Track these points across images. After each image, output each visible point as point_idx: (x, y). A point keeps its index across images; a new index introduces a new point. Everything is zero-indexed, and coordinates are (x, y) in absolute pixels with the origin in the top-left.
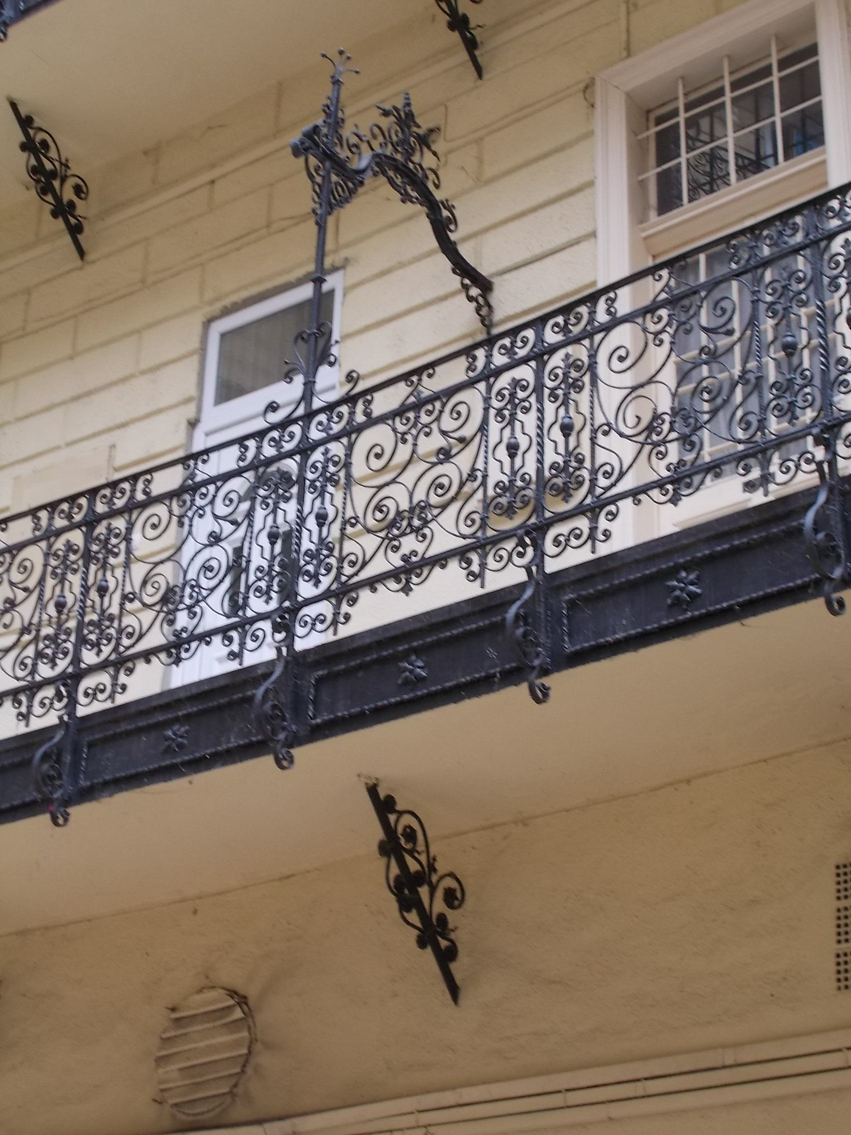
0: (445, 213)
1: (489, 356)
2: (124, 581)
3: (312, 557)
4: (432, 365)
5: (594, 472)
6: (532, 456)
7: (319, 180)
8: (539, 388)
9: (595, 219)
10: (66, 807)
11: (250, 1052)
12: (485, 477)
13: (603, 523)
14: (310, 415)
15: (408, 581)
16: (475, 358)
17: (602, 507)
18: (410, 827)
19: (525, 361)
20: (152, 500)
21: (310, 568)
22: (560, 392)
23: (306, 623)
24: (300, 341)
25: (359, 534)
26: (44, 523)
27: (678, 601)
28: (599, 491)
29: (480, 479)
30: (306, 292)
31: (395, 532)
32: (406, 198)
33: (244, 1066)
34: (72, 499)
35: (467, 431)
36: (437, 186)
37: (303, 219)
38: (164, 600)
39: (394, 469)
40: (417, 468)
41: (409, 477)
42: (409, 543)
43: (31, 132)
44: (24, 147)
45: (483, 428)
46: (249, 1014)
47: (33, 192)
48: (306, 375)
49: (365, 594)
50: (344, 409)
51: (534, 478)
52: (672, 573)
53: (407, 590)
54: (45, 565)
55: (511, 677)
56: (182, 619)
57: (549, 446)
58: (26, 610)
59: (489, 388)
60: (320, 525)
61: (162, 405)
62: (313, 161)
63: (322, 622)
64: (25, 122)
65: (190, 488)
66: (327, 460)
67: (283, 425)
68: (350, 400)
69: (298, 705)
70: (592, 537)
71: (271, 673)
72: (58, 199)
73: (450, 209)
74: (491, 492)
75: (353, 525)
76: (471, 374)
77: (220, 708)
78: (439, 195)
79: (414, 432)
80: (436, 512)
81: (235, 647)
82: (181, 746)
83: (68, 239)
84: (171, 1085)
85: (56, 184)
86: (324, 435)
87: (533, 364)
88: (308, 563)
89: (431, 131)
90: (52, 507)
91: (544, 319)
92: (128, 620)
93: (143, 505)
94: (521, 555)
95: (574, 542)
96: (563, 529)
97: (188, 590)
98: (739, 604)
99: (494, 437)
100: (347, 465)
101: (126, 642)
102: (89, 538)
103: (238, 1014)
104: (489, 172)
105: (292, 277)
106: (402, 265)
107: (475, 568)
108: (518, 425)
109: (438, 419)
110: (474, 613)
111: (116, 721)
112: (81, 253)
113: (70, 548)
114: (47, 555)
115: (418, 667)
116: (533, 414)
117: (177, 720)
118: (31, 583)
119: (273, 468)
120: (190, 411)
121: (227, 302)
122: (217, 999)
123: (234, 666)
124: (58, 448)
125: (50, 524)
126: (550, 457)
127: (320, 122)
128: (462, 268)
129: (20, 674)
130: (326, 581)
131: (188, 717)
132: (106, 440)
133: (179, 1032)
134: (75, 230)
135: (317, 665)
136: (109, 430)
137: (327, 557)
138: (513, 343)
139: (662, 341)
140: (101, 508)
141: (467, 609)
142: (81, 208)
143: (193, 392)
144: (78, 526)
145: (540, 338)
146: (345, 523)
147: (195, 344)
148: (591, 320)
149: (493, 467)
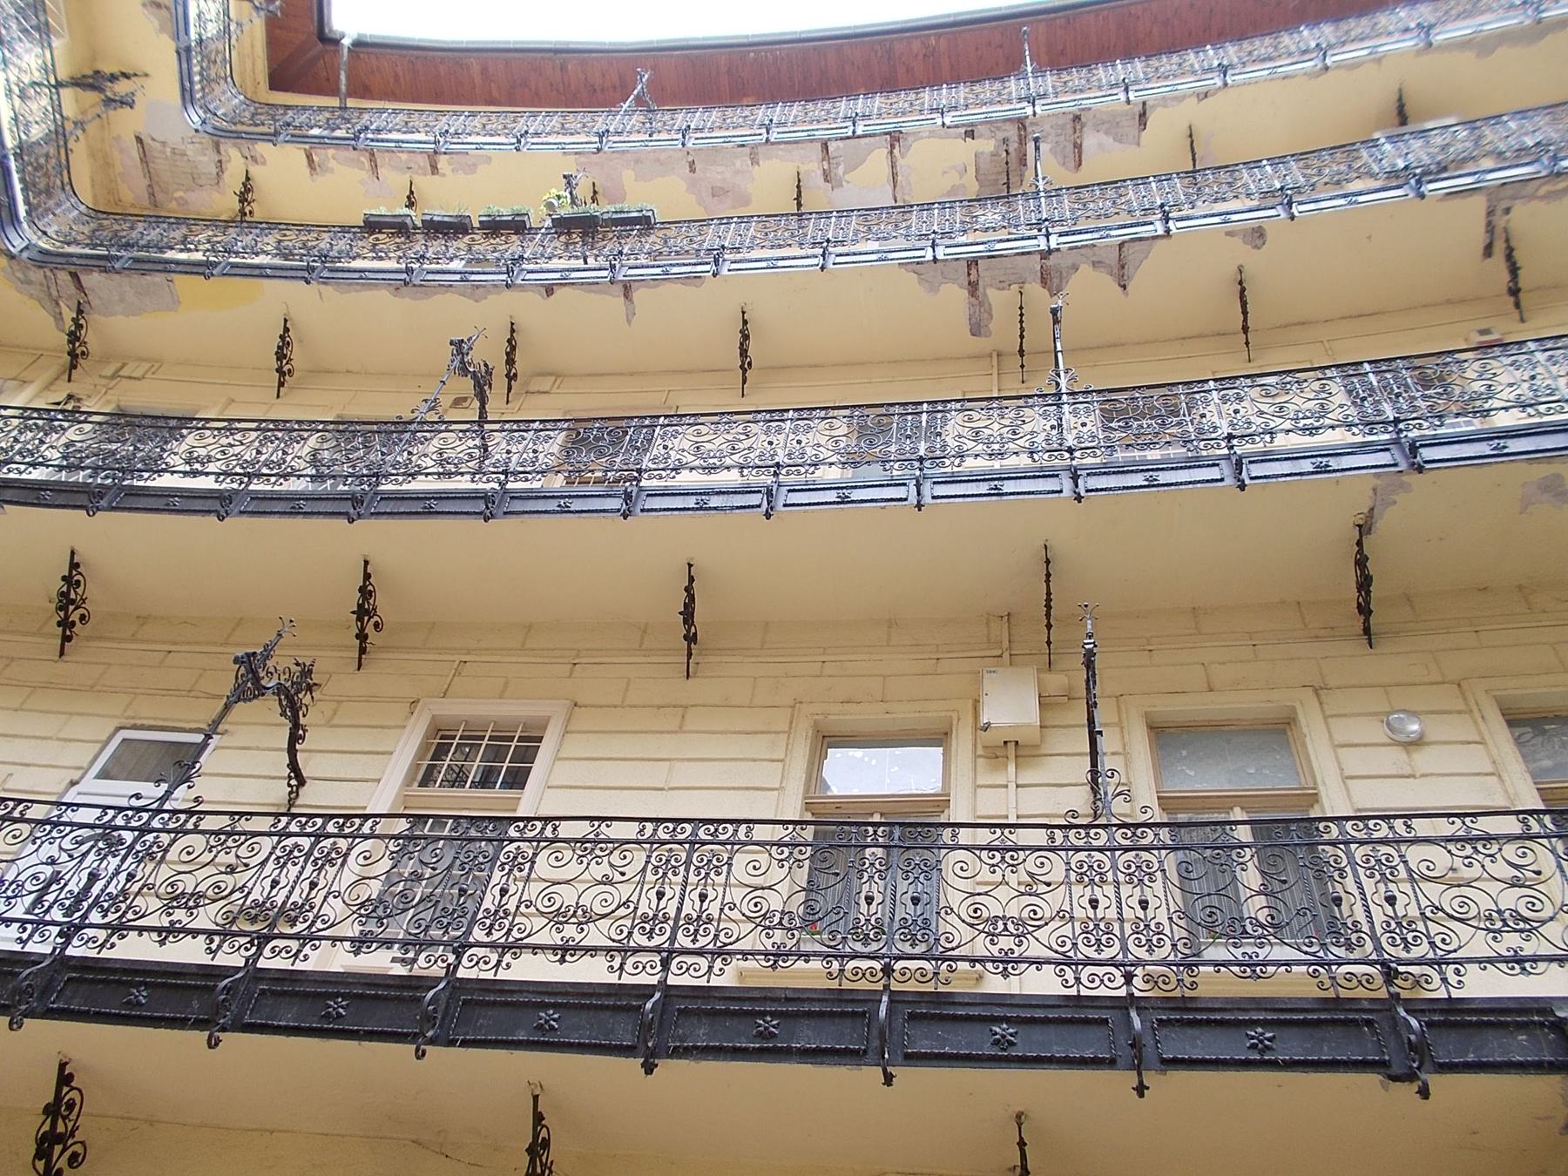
0: (301, 732)
1: (288, 824)
2: (523, 890)
4: (252, 814)
5: (317, 917)
6: (285, 892)
7: (240, 681)
8: (309, 854)
9: (383, 773)
12: (249, 893)
13: (307, 950)
14: (159, 811)
15: (166, 938)
17: (511, 948)
18: (74, 1100)
19: (309, 835)
20: (22, 820)
21: (106, 905)
22: (320, 862)
25: (150, 895)
27: (329, 1014)
28: (314, 929)
29: (631, 909)
30: (199, 738)
32: (283, 714)
36: (304, 716)
39: (633, 883)
40: (210, 870)
41: (201, 874)
42: (180, 915)
43: (74, 573)
45: (263, 863)
48: (170, 787)
49: (133, 934)
51: (279, 905)
52: (334, 996)
53: (162, 943)
55: (199, 1024)
57: (297, 890)
59: (279, 842)
60: (128, 881)
61: (59, 764)
64: (74, 566)
66: (155, 843)
68: (190, 813)
70: (296, 955)
72: (67, 617)
73: (305, 731)
74: (248, 902)
78: (302, 721)
80: (207, 901)
81: (25, 936)
83: (59, 641)
85: (71, 608)
86: (161, 826)
88: (105, 901)
89: (315, 684)
91: (332, 816)
92: (139, 901)
93: (15, 821)
94: (247, 949)
95: (283, 954)
96: (281, 943)
97: (14, 886)
98: (364, 1031)
100: (166, 851)
104: (336, 721)
106: (258, 748)
107: (214, 946)
108: (285, 870)
109: (239, 846)
110: (197, 974)
112: (62, 654)
115: (142, 996)
116: (298, 868)
119: (115, 834)
120: (76, 775)
121: (139, 722)
123: (17, 948)
126: (295, 898)
127: (258, 652)
128: (294, 766)
130: (111, 917)
132: (10, 769)
134: (66, 639)
135: (74, 969)
138: (307, 822)
139: (582, 862)
141: (195, 970)
142: (78, 628)
143: (85, 765)
145: (324, 826)
146: (144, 886)
147: (104, 738)
148: (359, 829)
149: (258, 888)
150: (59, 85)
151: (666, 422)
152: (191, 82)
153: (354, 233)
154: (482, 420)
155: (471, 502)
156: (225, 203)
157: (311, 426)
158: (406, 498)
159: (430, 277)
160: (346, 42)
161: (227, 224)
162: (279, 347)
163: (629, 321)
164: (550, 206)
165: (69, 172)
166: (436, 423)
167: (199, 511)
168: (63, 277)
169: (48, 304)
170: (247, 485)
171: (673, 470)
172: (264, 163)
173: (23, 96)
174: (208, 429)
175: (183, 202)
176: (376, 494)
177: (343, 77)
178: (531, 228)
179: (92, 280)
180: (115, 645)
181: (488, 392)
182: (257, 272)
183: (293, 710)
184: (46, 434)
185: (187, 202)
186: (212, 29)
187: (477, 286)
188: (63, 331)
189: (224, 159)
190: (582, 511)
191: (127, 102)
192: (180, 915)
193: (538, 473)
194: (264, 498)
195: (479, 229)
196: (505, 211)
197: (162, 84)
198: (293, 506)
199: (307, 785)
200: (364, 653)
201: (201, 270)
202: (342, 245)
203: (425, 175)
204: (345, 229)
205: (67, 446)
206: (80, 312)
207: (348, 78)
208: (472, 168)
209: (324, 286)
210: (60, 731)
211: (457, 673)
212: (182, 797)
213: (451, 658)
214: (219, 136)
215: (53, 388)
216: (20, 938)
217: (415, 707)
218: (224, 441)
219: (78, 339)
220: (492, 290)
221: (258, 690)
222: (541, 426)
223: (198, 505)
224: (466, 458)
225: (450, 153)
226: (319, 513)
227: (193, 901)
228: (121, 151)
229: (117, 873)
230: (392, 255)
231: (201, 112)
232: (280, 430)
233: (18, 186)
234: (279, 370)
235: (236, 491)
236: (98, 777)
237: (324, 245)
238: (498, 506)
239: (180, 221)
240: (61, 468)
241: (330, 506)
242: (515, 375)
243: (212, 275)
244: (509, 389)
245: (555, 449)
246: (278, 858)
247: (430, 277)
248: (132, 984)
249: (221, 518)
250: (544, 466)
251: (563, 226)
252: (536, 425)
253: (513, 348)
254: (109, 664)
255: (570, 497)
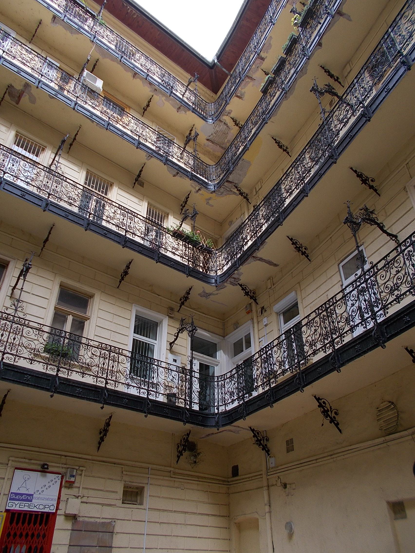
3: (375, 302)
10: (339, 368)
11: (398, 415)
12: (409, 273)
16: (398, 250)
20: (337, 301)
23: (378, 316)
24: (358, 260)
26: (317, 312)
30: (357, 252)
31: (392, 291)
33: (398, 418)
34: (321, 306)
35: (401, 265)
37: (352, 238)
38: (346, 320)
44: (292, 244)
45: (405, 263)
46: (395, 406)
47: (297, 252)
50: (372, 270)
54: (320, 321)
56: (352, 323)
58: (319, 330)
59: (403, 255)
60: (375, 295)
62: (349, 224)
63: (382, 315)
64: (291, 239)
65: (344, 296)
66: (372, 281)
67: (360, 277)
68: (372, 267)
69: (382, 334)
71: (374, 329)
72: (302, 252)
73: (382, 224)
75: (382, 293)
76: (398, 253)
77: (365, 339)
78: (379, 222)
79: (389, 269)
82: (360, 349)
84: (382, 426)
85: (301, 249)
86: (369, 277)
87: (411, 246)
88: (374, 304)
89: (373, 211)
90: (318, 309)
97: (350, 317)
99: (408, 264)
101: (341, 331)
102: (327, 313)
103: (392, 406)
105: (353, 250)
106: (376, 239)
111: (344, 348)
112: (310, 260)
113: (324, 316)
114: (320, 319)
117: (357, 344)
118: (318, 325)
120: (340, 283)
121: (341, 259)
122: (386, 404)
124: (317, 299)
125: (319, 312)
129: (322, 344)
130: (380, 306)
131: (359, 343)
133: (380, 413)
134: (307, 256)
135: (384, 324)
136: (325, 292)
137: (378, 301)
138: (405, 243)
140: (328, 306)
144: (324, 311)
146: (380, 293)
147: (337, 270)
149: (410, 270)
150: (184, 148)
151: (392, 29)
152: (202, 115)
153: (263, 98)
154: (340, 98)
155: (360, 122)
156: (235, 130)
157: (303, 153)
158: (343, 141)
159: (289, 84)
160: (216, 61)
161: (240, 132)
162: (278, 145)
163: (350, 20)
164: (296, 24)
165: (204, 162)
166: (329, 114)
167: (301, 200)
168: (226, 184)
169: (229, 193)
170: (304, 183)
171: (409, 38)
172: (232, 111)
173: (182, 158)
174: (283, 180)
175: (228, 141)
176: (334, 149)
177: (224, 70)
178: (298, 37)
179: (231, 178)
180: (318, 248)
181: (335, 91)
182: (255, 135)
183: (373, 222)
184: (257, 219)
185: (229, 140)
186: (193, 98)
187: (302, 70)
188: (238, 195)
189: (224, 121)
190: (394, 85)
191: (197, 135)
192: (396, 293)
193: (370, 91)
194: (311, 181)
195: (287, 56)
196: (287, 43)
197: (199, 123)
198: (319, 175)
199: (398, 236)
200: (377, 191)
201: (245, 150)
202: (264, 105)
203: (262, 63)
204: (261, 101)
205: (262, 216)
206: (236, 187)
207: (225, 68)
208: (270, 46)
209: (271, 119)
210: (327, 277)
211: (408, 169)
212: (367, 267)
213: (402, 166)
214: (217, 118)
215: (249, 209)
216: (364, 327)
217: (406, 189)
218: (289, 179)
219: (242, 193)
220: (306, 65)
221: (358, 225)
222: (357, 79)
223: (299, 199)
224: (346, 113)
225: (261, 50)
226: (326, 170)
227: (397, 287)
228: (208, 146)
229: (370, 295)
230: (276, 91)
231: (210, 118)
232: (297, 162)
233: (201, 177)
234: (284, 150)
235: (304, 187)
236: (345, 280)
237: (261, 111)
238: (369, 113)
239: (231, 145)
240: (266, 222)
241: (327, 166)
242: (337, 78)
243: (248, 148)
244: (340, 83)
245: (368, 79)
246: (407, 259)
247: (289, 84)
248: (402, 318)
249: (307, 196)
250: (369, 88)
251: (304, 24)
252: (355, 81)
253: (329, 72)
254: (321, 253)
255: (386, 85)
